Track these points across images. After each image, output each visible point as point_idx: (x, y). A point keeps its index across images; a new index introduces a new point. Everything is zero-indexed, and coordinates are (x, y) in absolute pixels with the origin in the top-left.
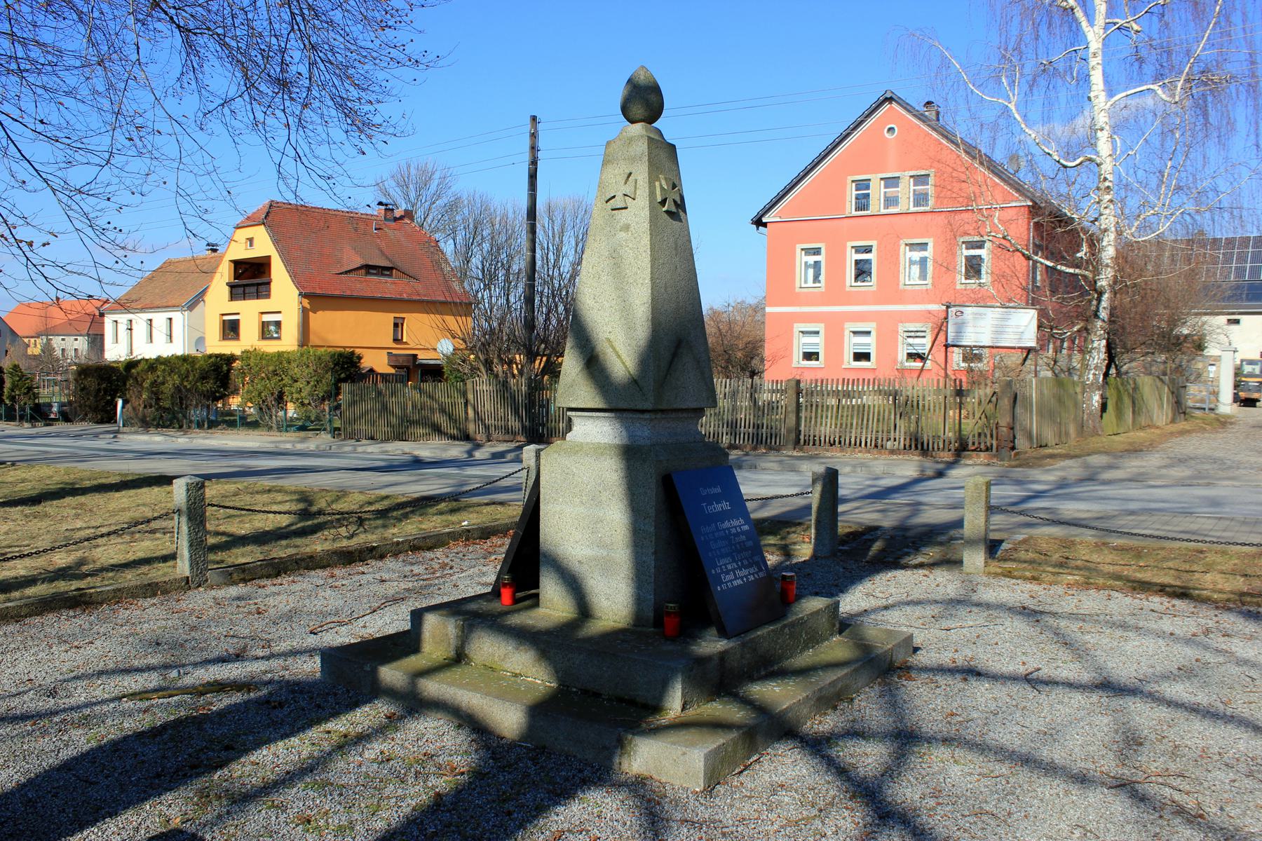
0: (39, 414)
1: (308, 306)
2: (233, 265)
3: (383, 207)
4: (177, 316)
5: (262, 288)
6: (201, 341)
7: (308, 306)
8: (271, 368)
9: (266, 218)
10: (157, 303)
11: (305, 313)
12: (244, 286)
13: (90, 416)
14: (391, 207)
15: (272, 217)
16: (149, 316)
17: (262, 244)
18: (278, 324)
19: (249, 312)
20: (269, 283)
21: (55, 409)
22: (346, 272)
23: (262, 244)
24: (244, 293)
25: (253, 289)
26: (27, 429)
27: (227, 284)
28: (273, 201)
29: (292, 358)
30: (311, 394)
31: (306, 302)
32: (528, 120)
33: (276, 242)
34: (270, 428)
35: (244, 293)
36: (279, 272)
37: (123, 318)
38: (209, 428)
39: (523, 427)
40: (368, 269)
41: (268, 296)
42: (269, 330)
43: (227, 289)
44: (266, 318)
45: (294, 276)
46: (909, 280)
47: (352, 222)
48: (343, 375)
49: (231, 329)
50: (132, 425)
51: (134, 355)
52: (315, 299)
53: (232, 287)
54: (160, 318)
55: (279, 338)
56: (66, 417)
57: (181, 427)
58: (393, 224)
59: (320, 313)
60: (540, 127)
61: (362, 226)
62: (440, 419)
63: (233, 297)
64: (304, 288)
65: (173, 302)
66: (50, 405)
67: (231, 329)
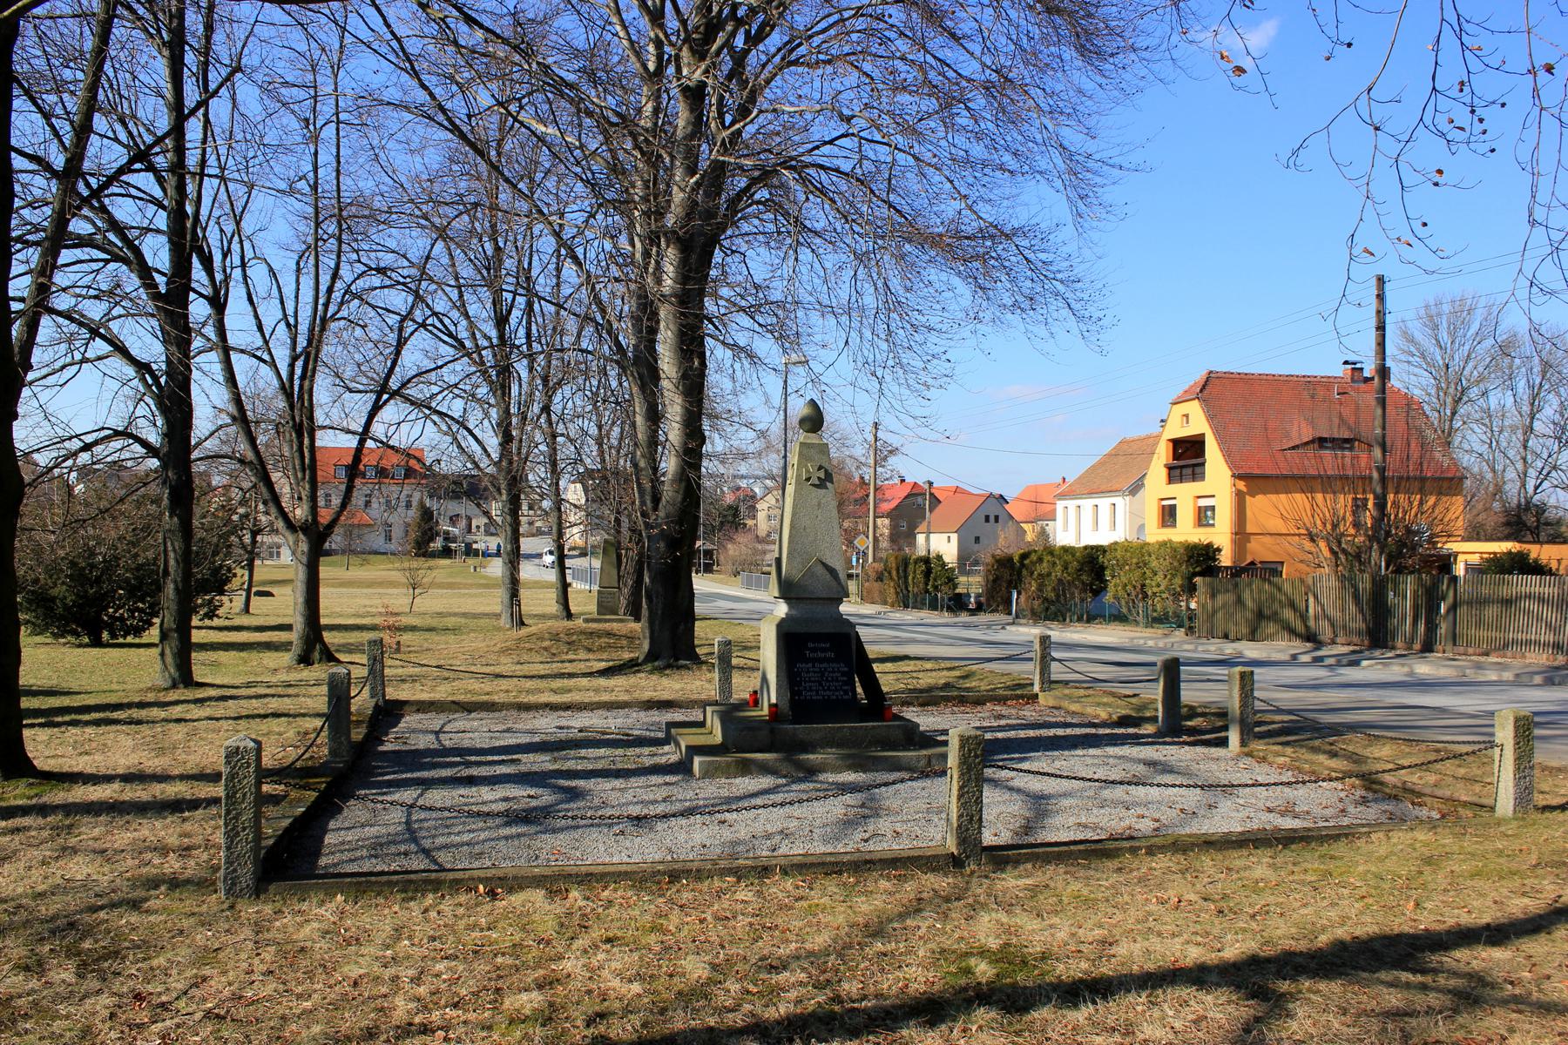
0: (958, 604)
1: (1245, 489)
2: (1171, 445)
3: (1349, 367)
4: (1119, 501)
5: (1198, 470)
6: (1141, 528)
7: (1245, 489)
8: (1134, 561)
9: (1201, 391)
10: (1103, 487)
11: (1240, 498)
12: (1182, 467)
13: (1001, 608)
14: (1358, 366)
15: (1211, 389)
16: (1113, 500)
17: (1195, 421)
18: (1213, 508)
19: (1185, 495)
20: (1203, 464)
21: (972, 600)
22: (1293, 448)
23: (1195, 421)
24: (1194, 474)
25: (1189, 471)
26: (946, 617)
27: (1166, 466)
28: (1211, 372)
29: (1151, 550)
30: (1167, 588)
31: (1241, 485)
32: (1374, 282)
33: (1211, 418)
34: (1137, 623)
35: (1194, 474)
36: (1213, 452)
37: (1071, 504)
38: (1088, 621)
39: (1368, 628)
40: (1321, 442)
41: (1202, 478)
42: (1204, 516)
43: (1164, 472)
44: (1203, 503)
45: (1228, 455)
46: (288, 628)
47: (1311, 387)
48: (1198, 569)
49: (1168, 515)
50: (1024, 617)
51: (497, 609)
52: (1252, 481)
53: (1170, 468)
54: (1104, 503)
55: (1213, 525)
56: (980, 608)
57: (1065, 620)
58: (1362, 385)
59: (1259, 497)
60: (1388, 286)
61: (1321, 393)
62: (1288, 614)
63: (1171, 480)
64: (1237, 468)
65: (1117, 486)
66: (968, 595)
67: (1168, 515)
